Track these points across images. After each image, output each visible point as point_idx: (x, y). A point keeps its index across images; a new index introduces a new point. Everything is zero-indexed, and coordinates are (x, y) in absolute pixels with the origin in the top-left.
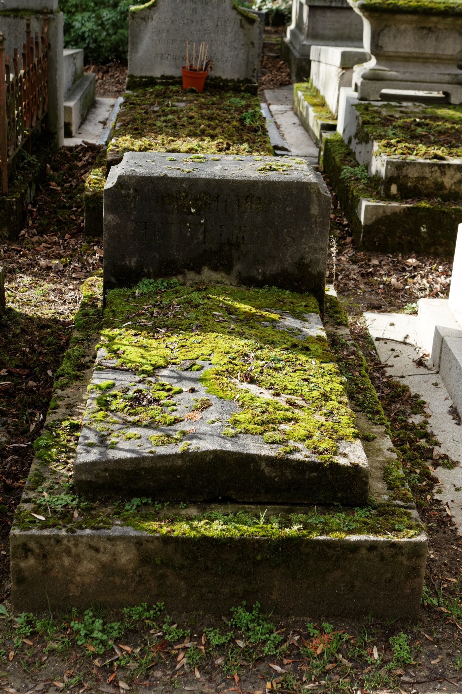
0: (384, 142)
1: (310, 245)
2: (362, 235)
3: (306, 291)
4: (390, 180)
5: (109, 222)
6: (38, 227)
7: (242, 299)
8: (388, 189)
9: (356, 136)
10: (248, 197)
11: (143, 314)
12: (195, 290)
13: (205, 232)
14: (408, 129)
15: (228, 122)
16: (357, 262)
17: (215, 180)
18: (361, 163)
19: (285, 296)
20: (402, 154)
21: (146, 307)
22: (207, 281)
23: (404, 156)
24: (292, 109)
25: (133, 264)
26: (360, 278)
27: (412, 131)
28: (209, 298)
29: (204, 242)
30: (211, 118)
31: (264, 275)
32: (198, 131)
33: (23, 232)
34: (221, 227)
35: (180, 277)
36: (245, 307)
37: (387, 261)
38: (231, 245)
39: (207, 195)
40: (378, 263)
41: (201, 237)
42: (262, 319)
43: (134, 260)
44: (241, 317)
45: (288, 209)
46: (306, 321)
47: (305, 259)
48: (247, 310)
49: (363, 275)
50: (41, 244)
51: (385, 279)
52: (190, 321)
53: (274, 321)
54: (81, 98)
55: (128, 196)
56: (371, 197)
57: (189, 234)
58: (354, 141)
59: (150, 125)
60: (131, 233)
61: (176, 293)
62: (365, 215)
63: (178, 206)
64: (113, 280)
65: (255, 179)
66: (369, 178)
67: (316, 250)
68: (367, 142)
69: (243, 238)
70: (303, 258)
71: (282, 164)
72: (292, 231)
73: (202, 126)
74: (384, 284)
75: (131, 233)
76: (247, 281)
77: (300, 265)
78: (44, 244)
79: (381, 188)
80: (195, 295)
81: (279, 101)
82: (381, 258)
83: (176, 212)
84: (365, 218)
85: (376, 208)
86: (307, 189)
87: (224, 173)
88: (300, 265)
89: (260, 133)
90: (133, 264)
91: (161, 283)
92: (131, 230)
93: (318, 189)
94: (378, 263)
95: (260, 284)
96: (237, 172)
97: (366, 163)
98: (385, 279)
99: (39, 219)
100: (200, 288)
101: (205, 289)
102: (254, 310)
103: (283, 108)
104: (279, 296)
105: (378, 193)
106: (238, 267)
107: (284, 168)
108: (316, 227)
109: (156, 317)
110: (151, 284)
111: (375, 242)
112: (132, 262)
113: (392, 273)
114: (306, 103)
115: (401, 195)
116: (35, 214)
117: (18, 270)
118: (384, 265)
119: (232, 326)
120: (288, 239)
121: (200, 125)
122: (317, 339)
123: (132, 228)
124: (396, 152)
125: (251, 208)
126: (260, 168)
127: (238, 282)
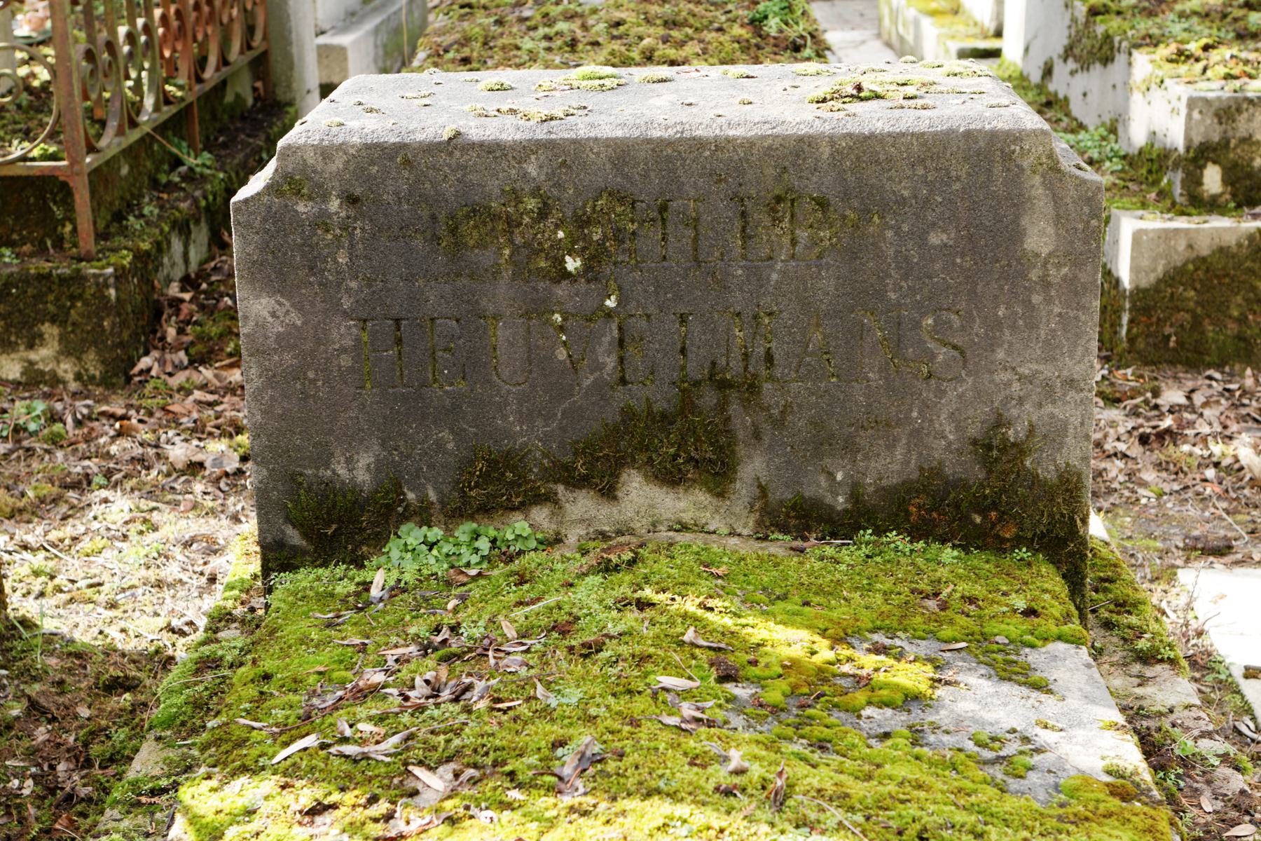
0: (1164, 51)
1: (1024, 370)
2: (1125, 319)
3: (1018, 542)
4: (1200, 155)
5: (261, 325)
6: (192, 344)
7: (772, 599)
8: (1193, 180)
9: (1068, 53)
10: (779, 199)
11: (374, 691)
12: (593, 571)
13: (621, 343)
14: (1224, 16)
15: (720, 30)
16: (1119, 401)
17: (649, 141)
18: (1090, 121)
19: (943, 573)
20: (1229, 77)
21: (391, 655)
22: (640, 525)
23: (1237, 83)
24: (879, 35)
25: (363, 476)
26: (1136, 450)
27: (1236, 20)
28: (642, 605)
29: (623, 381)
30: (671, 24)
31: (855, 496)
32: (636, 55)
33: (145, 362)
34: (683, 319)
35: (540, 514)
36: (787, 640)
37: (1209, 392)
38: (724, 385)
39: (621, 200)
40: (1183, 401)
41: (611, 362)
42: (861, 697)
43: (365, 460)
44: (774, 695)
45: (935, 239)
46: (1041, 687)
47: (1009, 424)
48: (797, 652)
49: (1144, 440)
50: (189, 393)
51: (1217, 449)
52: (557, 731)
53: (911, 699)
54: (376, 31)
55: (322, 222)
56: (1144, 205)
57: (562, 354)
58: (1062, 71)
59: (503, 48)
60: (346, 361)
61: (522, 582)
62: (1133, 258)
63: (516, 250)
64: (294, 537)
65: (804, 130)
66: (1124, 157)
67: (1048, 388)
68: (1107, 60)
69: (769, 358)
70: (1000, 422)
71: (901, 79)
72: (956, 321)
73: (646, 42)
74: (1217, 465)
75: (346, 361)
76: (798, 519)
77: (989, 447)
78: (198, 395)
79: (1174, 180)
80: (589, 595)
81: (846, 22)
82: (1190, 384)
83: (507, 274)
84: (1135, 269)
85: (1167, 236)
86: (1008, 157)
87: (684, 116)
88: (989, 447)
89: (807, 52)
90: (363, 476)
91: (467, 542)
92: (344, 350)
93: (1051, 155)
94: (1183, 401)
95: (840, 527)
96: (733, 112)
97: (1107, 119)
98: (1217, 449)
99: (196, 323)
100: (613, 557)
101: (632, 563)
102: (825, 653)
103: (856, 35)
104: (920, 572)
105: (1162, 194)
106: (753, 468)
107: (910, 91)
108: (1048, 301)
109: (421, 709)
110: (431, 546)
111: (1169, 337)
112: (358, 469)
113: (1234, 427)
114: (911, 13)
115: (1234, 195)
116: (185, 308)
117: (99, 479)
118: (1206, 404)
119: (736, 758)
120: (942, 354)
121: (641, 38)
122: (1114, 791)
123: (349, 342)
124: (1209, 73)
125: (794, 242)
126: (820, 94)
127: (759, 523)
